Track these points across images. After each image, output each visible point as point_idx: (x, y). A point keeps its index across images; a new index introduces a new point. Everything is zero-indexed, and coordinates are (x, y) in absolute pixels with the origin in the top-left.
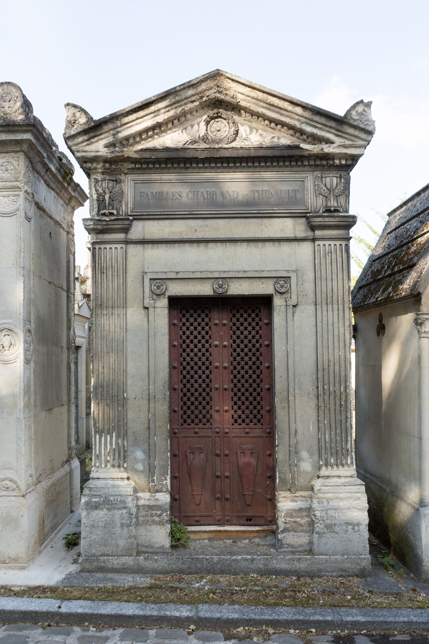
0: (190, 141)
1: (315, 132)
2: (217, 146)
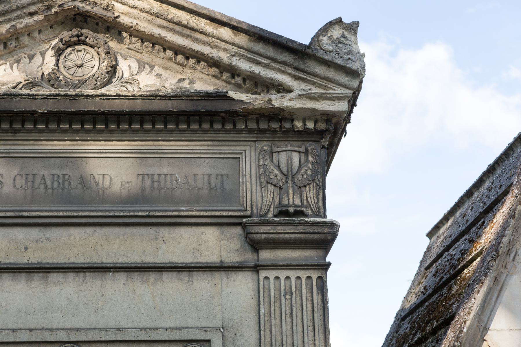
0: (24, 83)
1: (257, 72)
2: (71, 92)
